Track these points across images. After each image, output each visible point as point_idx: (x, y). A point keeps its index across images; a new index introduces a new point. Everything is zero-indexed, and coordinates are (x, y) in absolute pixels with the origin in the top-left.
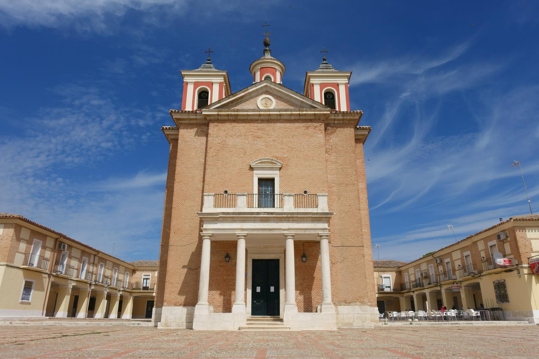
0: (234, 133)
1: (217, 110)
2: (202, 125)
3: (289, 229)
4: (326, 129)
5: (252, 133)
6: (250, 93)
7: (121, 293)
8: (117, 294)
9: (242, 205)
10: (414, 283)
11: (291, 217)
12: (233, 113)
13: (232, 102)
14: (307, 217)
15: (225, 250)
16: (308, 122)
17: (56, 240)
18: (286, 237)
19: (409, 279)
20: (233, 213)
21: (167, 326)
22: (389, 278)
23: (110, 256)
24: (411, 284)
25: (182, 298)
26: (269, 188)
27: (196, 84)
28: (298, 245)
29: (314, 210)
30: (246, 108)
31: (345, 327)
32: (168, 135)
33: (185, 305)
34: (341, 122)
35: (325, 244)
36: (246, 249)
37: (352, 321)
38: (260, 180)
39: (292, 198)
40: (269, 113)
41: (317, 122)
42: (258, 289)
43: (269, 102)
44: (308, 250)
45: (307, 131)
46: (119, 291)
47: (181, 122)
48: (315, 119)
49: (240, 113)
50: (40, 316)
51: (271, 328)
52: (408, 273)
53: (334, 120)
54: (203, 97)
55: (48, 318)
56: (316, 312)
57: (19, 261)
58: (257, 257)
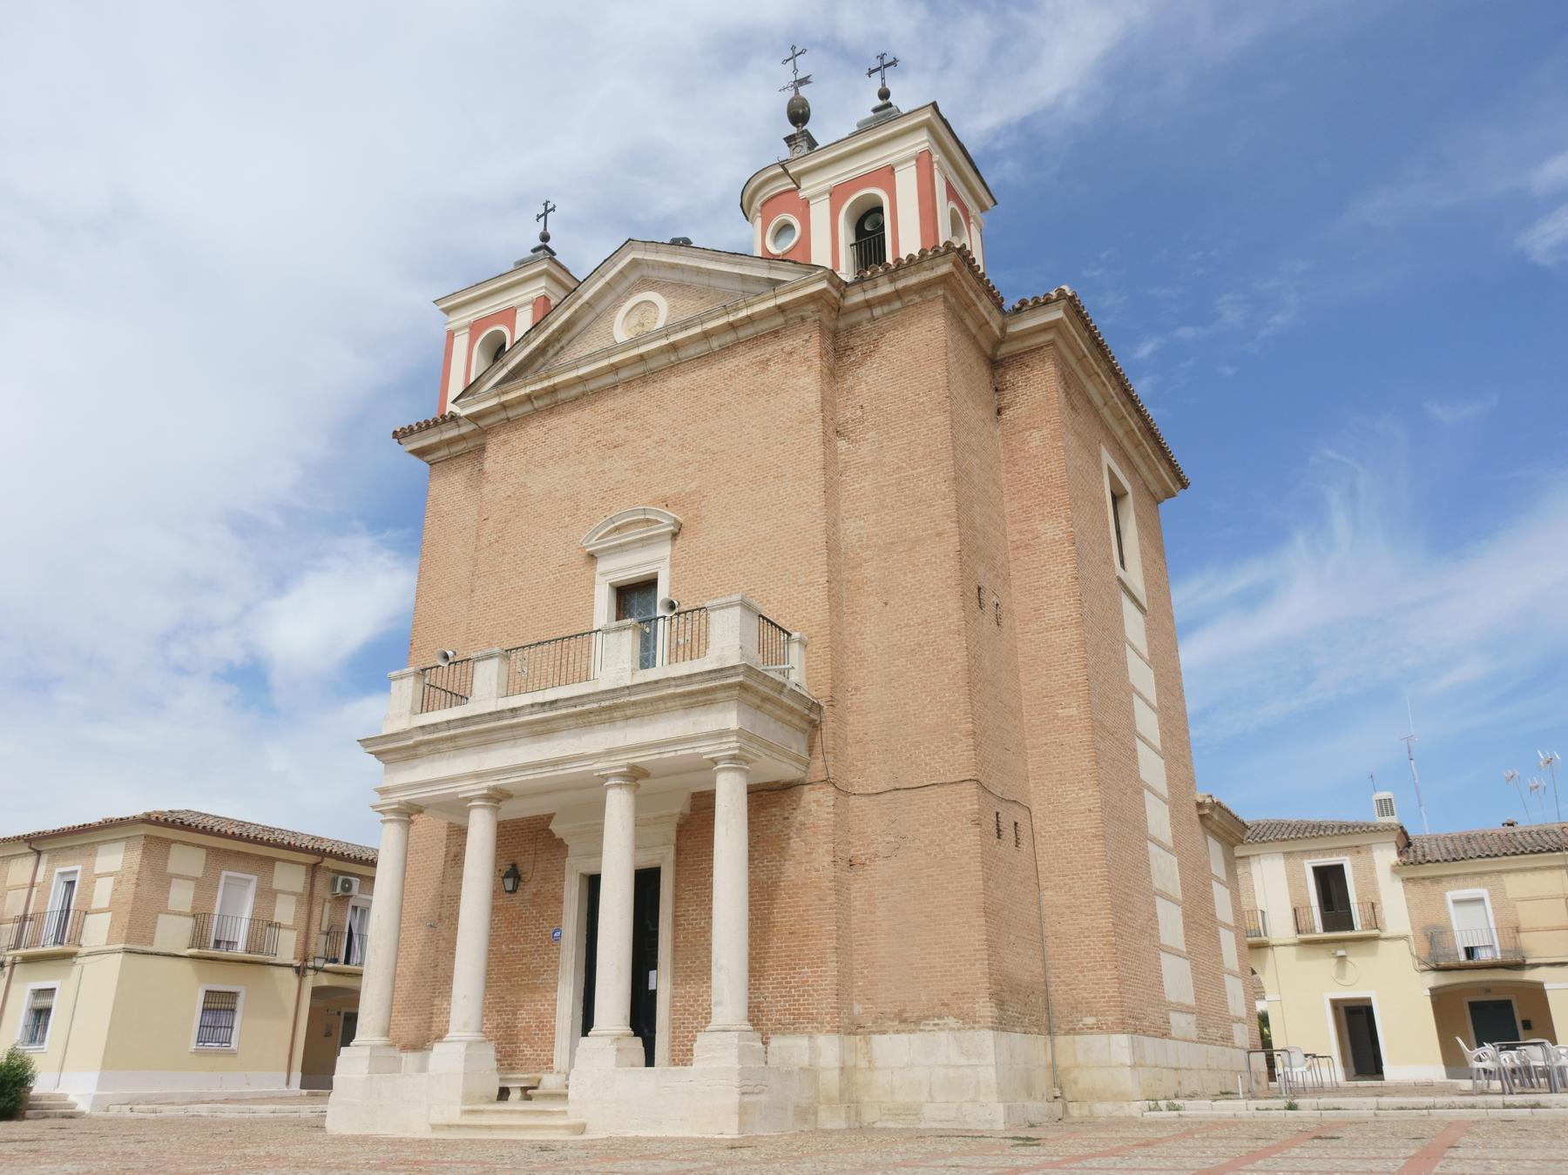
3: (609, 753)
5: (598, 437)
11: (616, 707)
14: (662, 699)
17: (314, 869)
22: (1481, 900)
27: (836, 195)
31: (891, 1125)
50: (278, 1087)
53: (869, 304)
55: (305, 1092)
57: (173, 932)
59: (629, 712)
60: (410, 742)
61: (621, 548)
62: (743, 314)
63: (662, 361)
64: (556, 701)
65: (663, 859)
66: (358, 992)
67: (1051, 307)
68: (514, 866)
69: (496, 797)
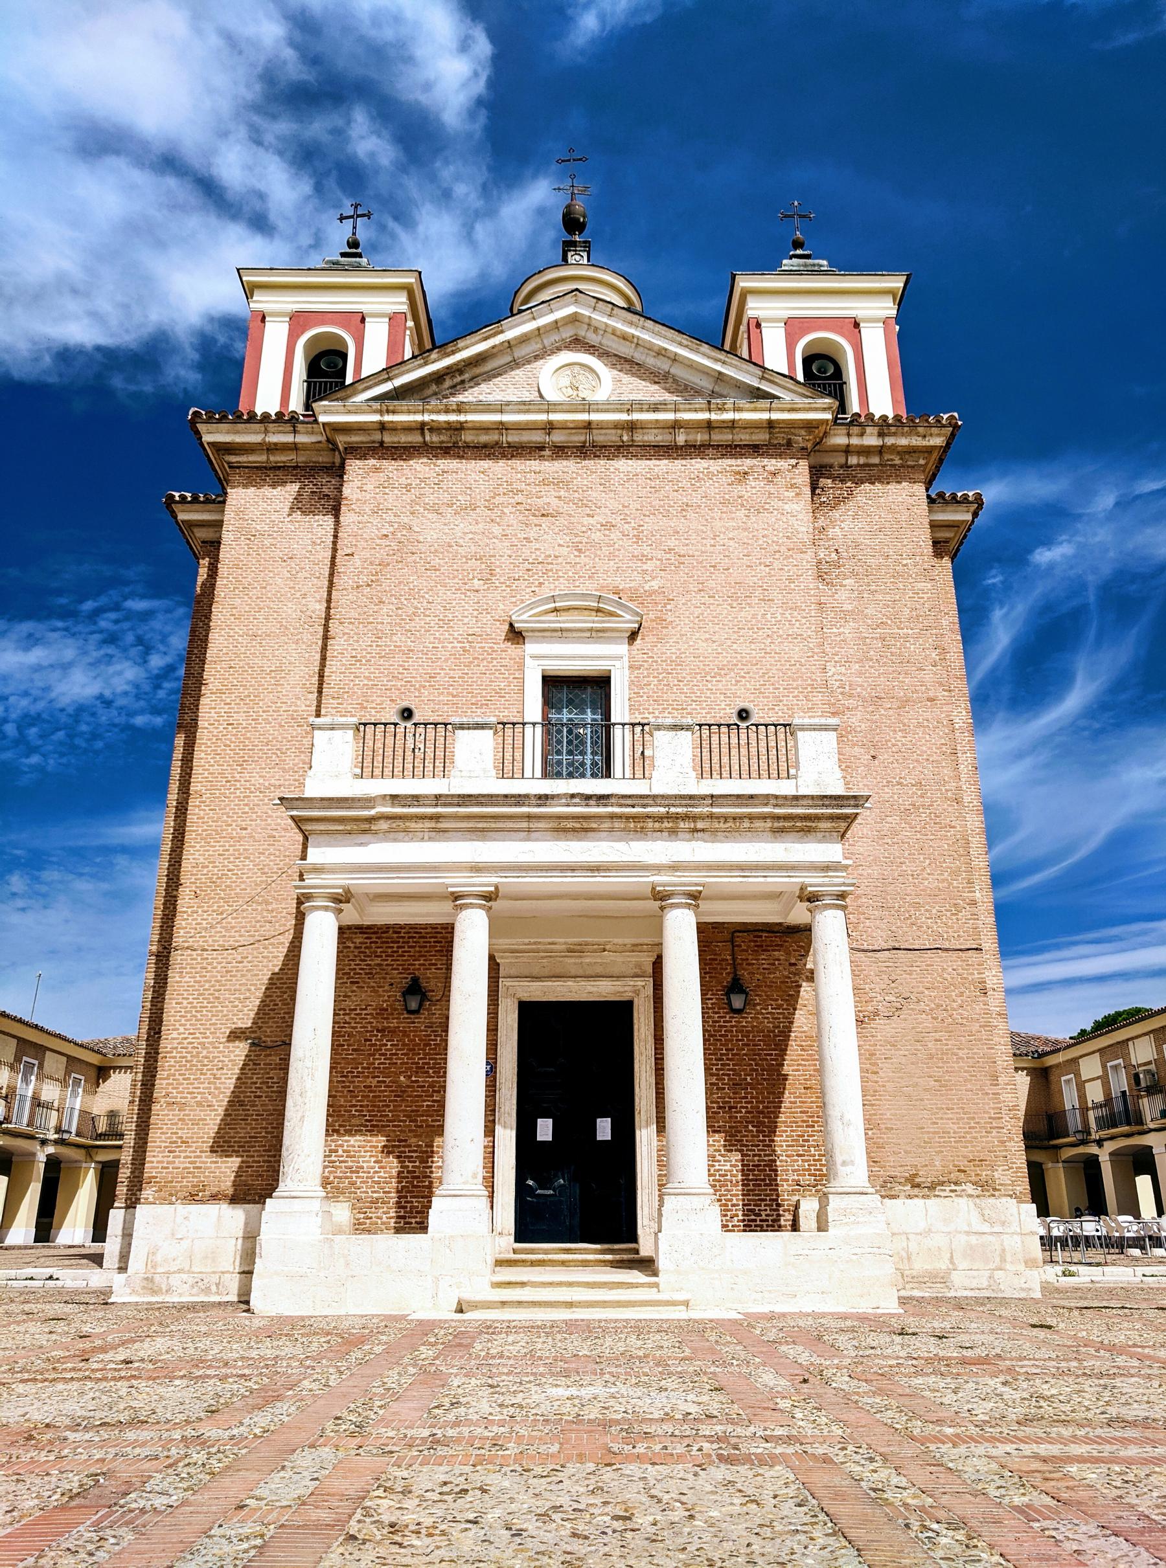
0: (446, 497)
1: (376, 405)
2: (319, 472)
3: (675, 867)
4: (814, 487)
5: (519, 498)
6: (509, 345)
7: (50, 1150)
8: (34, 1155)
9: (474, 764)
10: (1104, 1111)
11: (686, 817)
12: (443, 418)
13: (438, 378)
14: (751, 818)
15: (398, 967)
16: (742, 456)
18: (661, 897)
19: (1082, 1097)
20: (438, 797)
21: (154, 1292)
23: (20, 1021)
24: (1091, 1115)
25: (226, 1169)
26: (589, 716)
27: (299, 321)
28: (712, 937)
29: (785, 788)
30: (497, 398)
31: (917, 1293)
32: (191, 524)
33: (235, 1199)
34: (875, 460)
35: (830, 930)
36: (492, 958)
37: (943, 1265)
38: (551, 682)
39: (686, 739)
40: (584, 417)
41: (780, 456)
42: (545, 1130)
43: (584, 380)
44: (754, 965)
45: (739, 489)
46: (44, 1142)
47: (233, 459)
48: (774, 441)
49: (470, 417)
51: (604, 1304)
52: (1078, 1075)
53: (847, 450)
54: (327, 370)
56: (795, 1227)
58: (538, 991)
59: (700, 825)
60: (373, 812)
61: (562, 634)
62: (729, 416)
63: (611, 437)
64: (608, 797)
65: (637, 992)
66: (1028, 1148)
67: (963, 507)
68: (415, 980)
69: (341, 899)
